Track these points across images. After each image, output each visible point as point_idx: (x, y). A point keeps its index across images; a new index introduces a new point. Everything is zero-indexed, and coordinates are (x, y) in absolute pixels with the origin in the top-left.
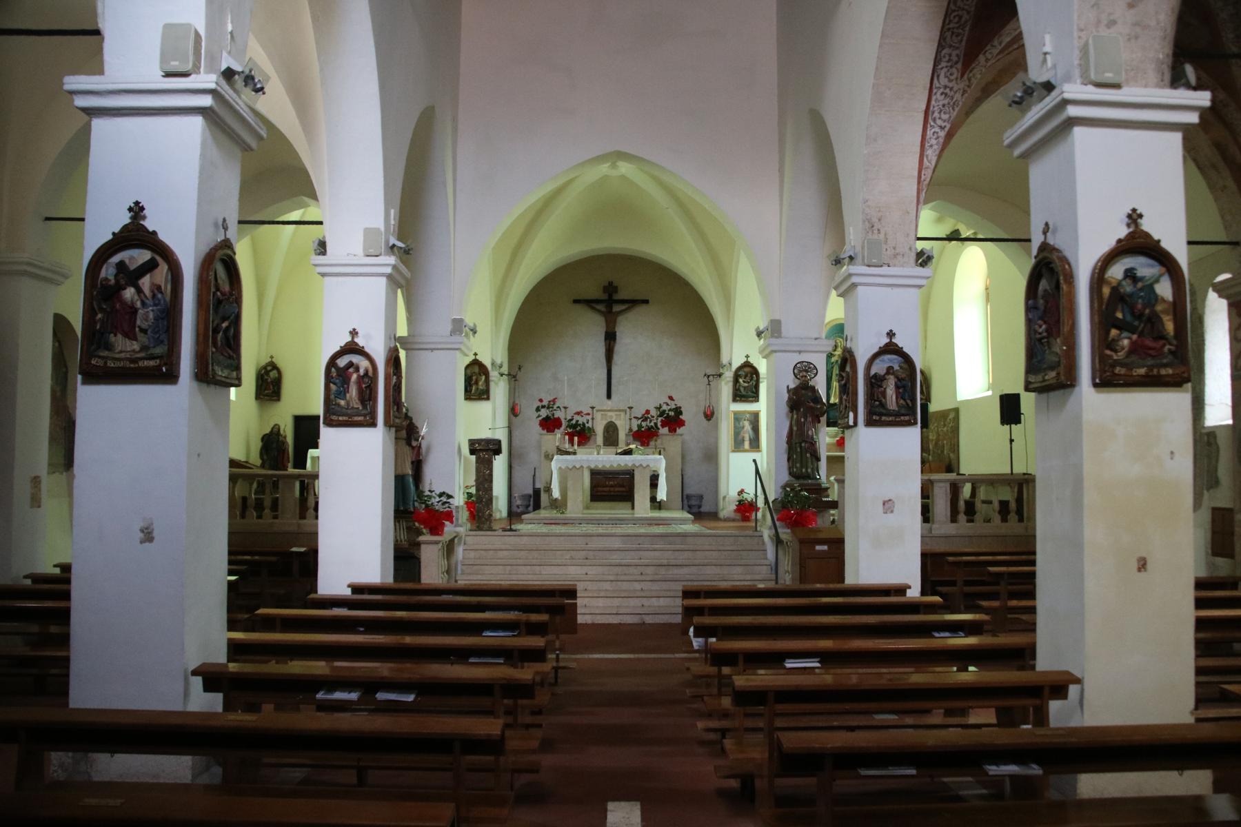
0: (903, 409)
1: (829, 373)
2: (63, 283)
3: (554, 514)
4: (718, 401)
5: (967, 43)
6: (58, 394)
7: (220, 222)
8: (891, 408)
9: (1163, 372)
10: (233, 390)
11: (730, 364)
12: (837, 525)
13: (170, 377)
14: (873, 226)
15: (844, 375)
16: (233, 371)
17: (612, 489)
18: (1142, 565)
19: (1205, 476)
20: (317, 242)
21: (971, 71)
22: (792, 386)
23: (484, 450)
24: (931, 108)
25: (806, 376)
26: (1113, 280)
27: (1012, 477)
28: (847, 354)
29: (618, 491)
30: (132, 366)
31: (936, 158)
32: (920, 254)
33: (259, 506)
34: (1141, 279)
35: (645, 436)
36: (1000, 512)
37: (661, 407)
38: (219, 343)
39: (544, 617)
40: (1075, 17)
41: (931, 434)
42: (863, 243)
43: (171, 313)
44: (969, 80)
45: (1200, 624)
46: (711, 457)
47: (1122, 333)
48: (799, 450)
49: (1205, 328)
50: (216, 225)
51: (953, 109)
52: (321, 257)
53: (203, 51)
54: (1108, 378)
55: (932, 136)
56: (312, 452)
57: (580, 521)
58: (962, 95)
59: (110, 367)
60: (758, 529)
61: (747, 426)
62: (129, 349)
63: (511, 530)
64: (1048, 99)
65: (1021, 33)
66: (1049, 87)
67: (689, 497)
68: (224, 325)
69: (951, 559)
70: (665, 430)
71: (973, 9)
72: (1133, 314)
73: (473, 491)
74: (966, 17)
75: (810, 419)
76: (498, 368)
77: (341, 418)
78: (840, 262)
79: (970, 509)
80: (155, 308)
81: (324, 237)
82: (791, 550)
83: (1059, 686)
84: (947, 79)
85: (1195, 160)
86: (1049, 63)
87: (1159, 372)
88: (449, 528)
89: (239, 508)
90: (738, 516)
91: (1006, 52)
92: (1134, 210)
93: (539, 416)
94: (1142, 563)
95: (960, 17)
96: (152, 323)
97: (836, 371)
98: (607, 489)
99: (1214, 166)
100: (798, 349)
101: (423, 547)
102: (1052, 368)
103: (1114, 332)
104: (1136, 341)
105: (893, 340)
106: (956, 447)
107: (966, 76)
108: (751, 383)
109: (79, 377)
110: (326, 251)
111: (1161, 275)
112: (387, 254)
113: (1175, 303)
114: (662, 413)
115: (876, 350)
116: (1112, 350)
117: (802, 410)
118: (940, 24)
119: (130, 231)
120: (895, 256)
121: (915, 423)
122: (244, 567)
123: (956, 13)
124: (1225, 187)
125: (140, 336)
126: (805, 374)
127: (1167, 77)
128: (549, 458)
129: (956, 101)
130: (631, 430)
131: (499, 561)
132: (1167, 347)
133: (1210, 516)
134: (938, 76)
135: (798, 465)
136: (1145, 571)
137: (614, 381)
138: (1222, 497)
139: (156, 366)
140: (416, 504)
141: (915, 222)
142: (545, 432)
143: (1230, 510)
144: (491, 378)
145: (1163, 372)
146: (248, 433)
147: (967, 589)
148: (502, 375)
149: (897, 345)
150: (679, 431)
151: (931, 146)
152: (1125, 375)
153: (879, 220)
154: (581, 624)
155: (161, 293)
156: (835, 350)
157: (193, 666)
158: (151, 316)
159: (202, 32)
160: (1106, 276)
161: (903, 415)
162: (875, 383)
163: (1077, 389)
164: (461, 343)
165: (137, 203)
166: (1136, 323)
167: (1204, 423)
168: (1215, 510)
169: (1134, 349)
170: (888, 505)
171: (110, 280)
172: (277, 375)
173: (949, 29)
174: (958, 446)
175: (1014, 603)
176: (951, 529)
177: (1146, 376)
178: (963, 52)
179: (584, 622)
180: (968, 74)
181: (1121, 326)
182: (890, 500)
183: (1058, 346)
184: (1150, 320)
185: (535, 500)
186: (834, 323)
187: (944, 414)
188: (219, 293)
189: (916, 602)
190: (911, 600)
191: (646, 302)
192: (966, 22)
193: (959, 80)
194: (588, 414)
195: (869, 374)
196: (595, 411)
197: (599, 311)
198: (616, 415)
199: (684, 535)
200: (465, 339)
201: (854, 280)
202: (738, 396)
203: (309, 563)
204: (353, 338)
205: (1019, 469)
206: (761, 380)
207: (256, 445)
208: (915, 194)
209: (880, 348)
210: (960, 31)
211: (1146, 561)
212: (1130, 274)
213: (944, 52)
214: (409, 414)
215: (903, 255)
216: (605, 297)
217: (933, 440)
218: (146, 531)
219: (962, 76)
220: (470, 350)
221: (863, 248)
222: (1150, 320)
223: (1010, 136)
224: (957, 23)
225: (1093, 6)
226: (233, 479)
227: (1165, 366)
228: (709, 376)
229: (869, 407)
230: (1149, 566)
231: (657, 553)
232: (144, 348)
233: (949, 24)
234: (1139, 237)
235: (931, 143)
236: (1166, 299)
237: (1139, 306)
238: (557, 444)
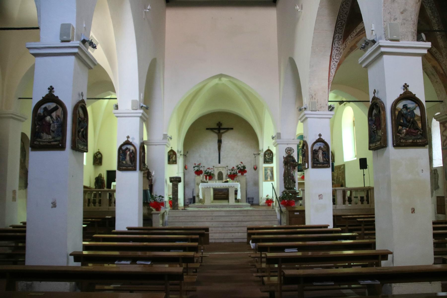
0: (325, 162)
1: (298, 152)
2: (24, 121)
3: (200, 204)
4: (258, 163)
5: (344, 32)
6: (23, 161)
7: (81, 93)
8: (321, 161)
9: (418, 141)
10: (85, 153)
11: (263, 150)
12: (303, 205)
13: (61, 147)
14: (313, 97)
15: (304, 150)
16: (85, 146)
17: (221, 196)
18: (413, 211)
19: (435, 185)
20: (115, 105)
21: (346, 41)
22: (285, 156)
23: (175, 181)
24: (332, 55)
25: (290, 153)
26: (399, 109)
27: (364, 188)
28: (305, 143)
29: (223, 196)
30: (49, 144)
31: (334, 72)
32: (330, 107)
33: (94, 203)
34: (409, 108)
35: (232, 176)
36: (360, 201)
37: (238, 166)
38: (80, 136)
39: (197, 236)
40: (382, 17)
41: (335, 174)
42: (310, 103)
43: (63, 125)
44: (346, 45)
45: (435, 258)
46: (256, 184)
47: (403, 128)
48: (288, 179)
49: (432, 132)
50: (79, 95)
51: (340, 55)
52: (116, 110)
53: (75, 33)
54: (399, 143)
55: (333, 65)
56: (113, 184)
57: (210, 207)
58: (343, 50)
59: (41, 145)
60: (274, 208)
61: (269, 172)
62: (48, 138)
63: (185, 209)
64: (374, 46)
65: (364, 27)
66: (374, 42)
67: (248, 198)
68: (82, 130)
69: (343, 217)
70: (240, 174)
71: (346, 20)
72: (406, 121)
73: (171, 196)
74: (344, 22)
75: (291, 168)
76: (179, 152)
77: (123, 168)
78: (301, 110)
79: (350, 200)
80: (57, 123)
81: (117, 104)
82: (286, 215)
83: (384, 256)
84: (337, 45)
85: (426, 72)
86: (374, 34)
87: (416, 141)
88: (162, 210)
89: (87, 202)
90: (267, 204)
91: (358, 35)
92: (406, 84)
93: (194, 170)
94: (413, 210)
95: (342, 23)
96: (56, 129)
97: (300, 152)
98: (219, 196)
99: (433, 74)
100: (287, 143)
101: (154, 216)
102: (378, 141)
103: (400, 127)
104: (408, 130)
105: (321, 137)
106: (344, 178)
107: (344, 44)
108: (270, 157)
109: (30, 148)
110: (118, 108)
111: (416, 107)
112: (140, 109)
113: (421, 117)
114: (238, 168)
115: (315, 141)
116: (399, 133)
117: (289, 165)
118: (335, 25)
119: (49, 96)
120: (321, 107)
121: (330, 167)
122: (89, 222)
123: (340, 21)
124: (437, 81)
125: (52, 133)
126: (289, 152)
127: (416, 38)
128: (198, 184)
129: (341, 52)
130: (227, 174)
131: (180, 221)
132: (419, 132)
133: (436, 200)
134: (335, 44)
135: (288, 184)
136: (414, 213)
137: (221, 157)
138: (440, 193)
139: (58, 144)
140: (151, 200)
141: (327, 95)
142: (197, 175)
143: (443, 197)
144: (177, 156)
145: (418, 141)
146: (90, 177)
147: (349, 228)
148: (181, 155)
149: (322, 139)
150: (245, 174)
151: (333, 68)
152: (404, 142)
153: (315, 95)
154: (210, 243)
155: (60, 118)
156: (300, 145)
157: (70, 252)
158: (56, 126)
159: (75, 27)
160: (397, 108)
161: (325, 164)
162: (315, 152)
163: (387, 148)
164: (166, 142)
165: (51, 87)
166: (408, 124)
167: (433, 166)
168: (438, 197)
169: (407, 133)
170: (320, 196)
171: (41, 114)
172: (100, 156)
173: (338, 27)
174: (345, 178)
175: (367, 232)
176: (344, 207)
177: (412, 142)
178: (343, 35)
179: (212, 242)
180: (345, 43)
181: (402, 125)
182: (321, 195)
183: (380, 133)
184: (413, 123)
185: (193, 200)
186: (299, 135)
187: (339, 167)
188: (80, 119)
189: (331, 230)
190: (330, 229)
191: (232, 129)
192: (344, 24)
193: (342, 45)
194: (212, 169)
195: (313, 150)
196: (214, 168)
197: (215, 132)
198: (222, 169)
199: (247, 211)
200: (168, 141)
201: (307, 116)
202: (266, 161)
203: (112, 222)
204: (128, 139)
205: (367, 185)
206: (274, 155)
207: (93, 181)
208: (327, 85)
209: (316, 140)
210: (342, 27)
211: (414, 209)
212: (405, 106)
213: (336, 35)
214: (148, 168)
215: (324, 107)
216: (217, 127)
217: (336, 176)
218: (53, 203)
219: (343, 43)
220: (170, 145)
221: (309, 105)
222: (413, 123)
223: (360, 60)
224: (341, 25)
225: (388, 13)
226: (85, 192)
227: (419, 139)
228: (255, 155)
229: (313, 161)
230: (415, 211)
231: (237, 217)
232: (53, 138)
233: (338, 25)
234: (408, 93)
235: (333, 67)
236: (418, 115)
237: (409, 118)
238: (201, 179)
